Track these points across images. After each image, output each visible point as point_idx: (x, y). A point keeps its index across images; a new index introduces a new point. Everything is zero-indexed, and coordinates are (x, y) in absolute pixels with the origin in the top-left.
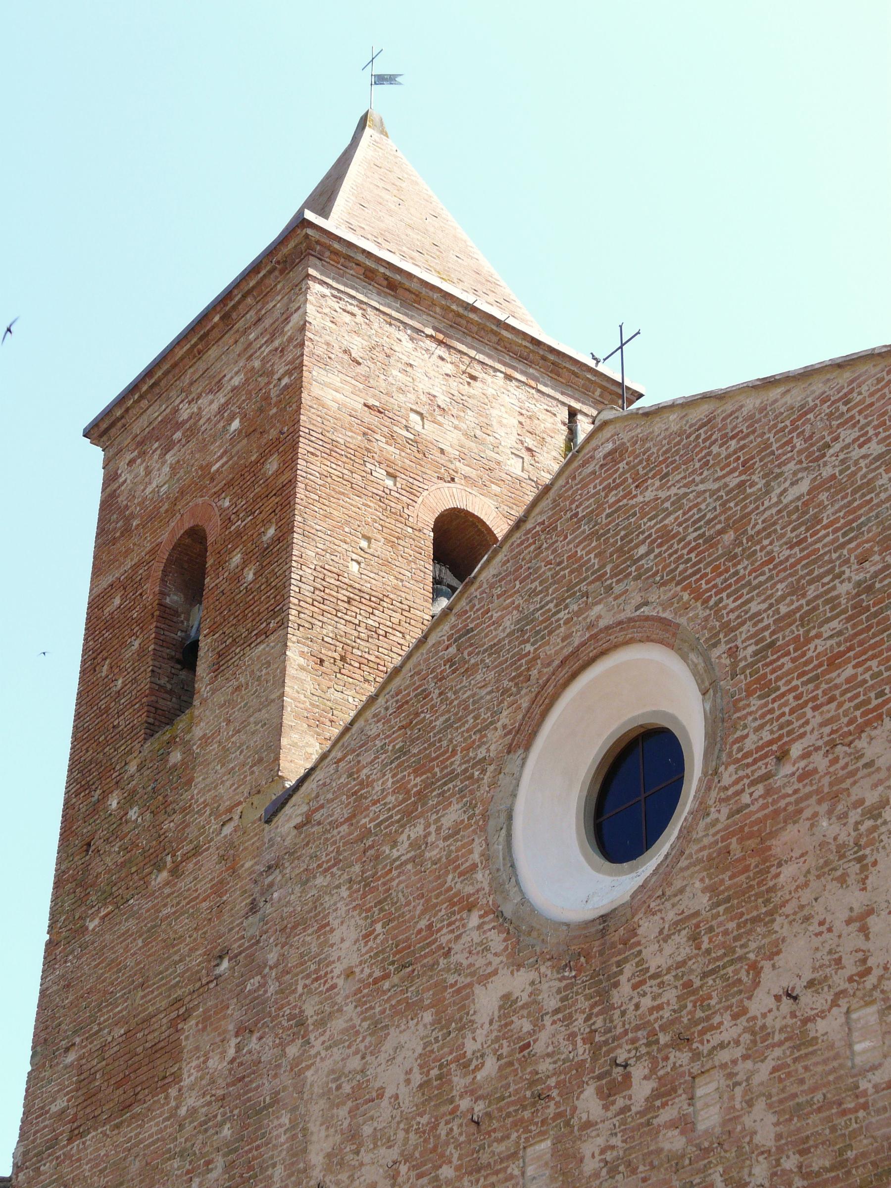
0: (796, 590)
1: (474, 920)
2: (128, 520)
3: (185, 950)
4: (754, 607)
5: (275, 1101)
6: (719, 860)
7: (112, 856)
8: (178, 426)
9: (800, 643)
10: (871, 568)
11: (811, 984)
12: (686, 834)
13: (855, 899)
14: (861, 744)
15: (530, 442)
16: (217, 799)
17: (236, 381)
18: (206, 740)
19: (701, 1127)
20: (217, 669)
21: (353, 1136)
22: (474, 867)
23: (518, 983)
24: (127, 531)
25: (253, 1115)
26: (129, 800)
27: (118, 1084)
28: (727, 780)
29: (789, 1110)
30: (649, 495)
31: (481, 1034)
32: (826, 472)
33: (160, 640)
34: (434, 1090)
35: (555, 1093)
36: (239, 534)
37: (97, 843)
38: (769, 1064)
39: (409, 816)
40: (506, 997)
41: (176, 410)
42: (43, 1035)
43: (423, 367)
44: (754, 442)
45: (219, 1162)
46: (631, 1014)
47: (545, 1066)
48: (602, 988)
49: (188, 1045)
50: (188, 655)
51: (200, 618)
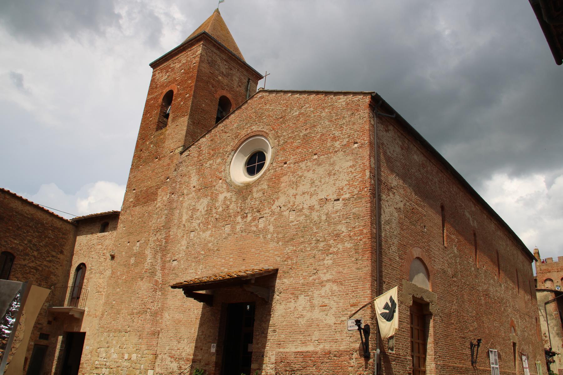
0: (293, 132)
1: (221, 181)
2: (157, 85)
4: (284, 134)
7: (145, 154)
8: (170, 68)
9: (292, 143)
10: (307, 132)
11: (284, 206)
12: (265, 173)
13: (294, 191)
14: (300, 164)
15: (240, 84)
16: (170, 147)
18: (169, 135)
19: (259, 227)
20: (173, 121)
21: (192, 217)
22: (222, 172)
23: (228, 195)
24: (156, 88)
26: (151, 143)
27: (144, 198)
28: (274, 165)
29: (276, 227)
30: (267, 107)
32: (302, 111)
34: (209, 212)
36: (181, 94)
38: (274, 218)
39: (210, 159)
40: (225, 197)
41: (170, 65)
44: (289, 102)
45: (164, 217)
46: (249, 205)
47: (231, 211)
49: (159, 194)
50: (167, 116)
51: (169, 110)
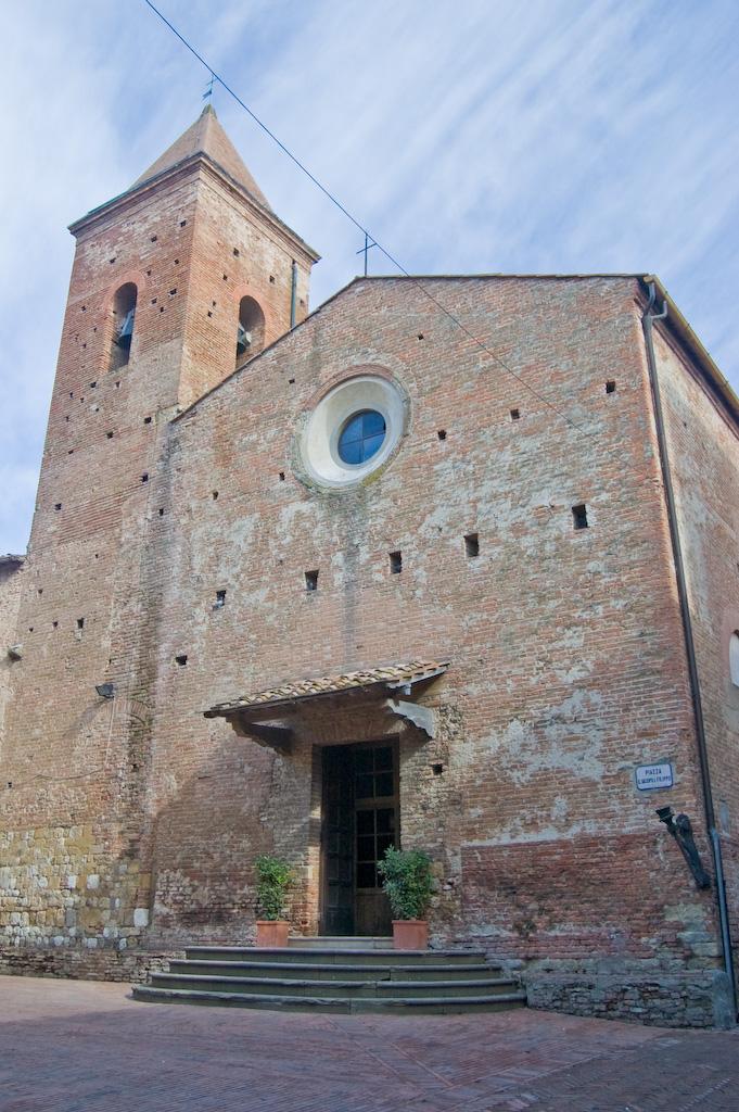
8: (121, 234)
17: (156, 220)
18: (135, 381)
20: (142, 350)
23: (305, 507)
24: (90, 278)
31: (285, 526)
34: (259, 547)
35: (321, 553)
43: (241, 230)
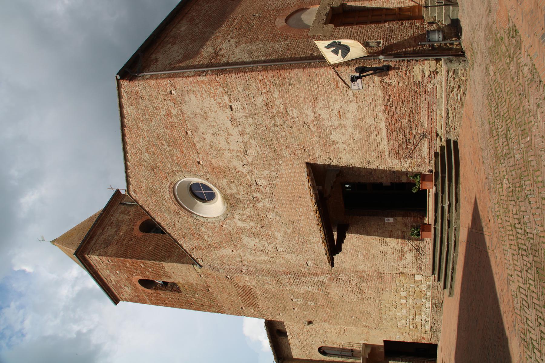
0: (167, 157)
2: (135, 296)
3: (225, 285)
4: (169, 166)
5: (255, 267)
6: (217, 177)
8: (116, 284)
9: (177, 158)
11: (242, 161)
13: (227, 152)
14: (198, 148)
15: (126, 212)
18: (184, 280)
19: (266, 184)
21: (262, 251)
23: (237, 217)
25: (258, 271)
26: (194, 296)
29: (264, 168)
30: (144, 185)
31: (246, 225)
32: (144, 150)
33: (161, 290)
34: (256, 235)
36: (141, 272)
37: (202, 303)
38: (255, 170)
40: (239, 220)
41: (113, 285)
42: (227, 213)
45: (265, 278)
48: (239, 201)
50: (165, 283)
